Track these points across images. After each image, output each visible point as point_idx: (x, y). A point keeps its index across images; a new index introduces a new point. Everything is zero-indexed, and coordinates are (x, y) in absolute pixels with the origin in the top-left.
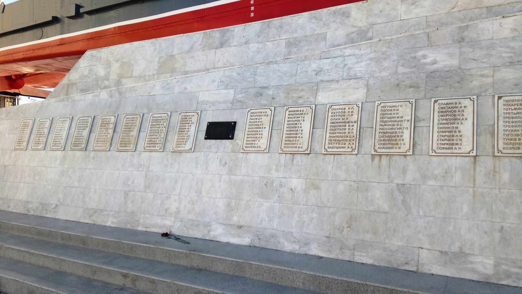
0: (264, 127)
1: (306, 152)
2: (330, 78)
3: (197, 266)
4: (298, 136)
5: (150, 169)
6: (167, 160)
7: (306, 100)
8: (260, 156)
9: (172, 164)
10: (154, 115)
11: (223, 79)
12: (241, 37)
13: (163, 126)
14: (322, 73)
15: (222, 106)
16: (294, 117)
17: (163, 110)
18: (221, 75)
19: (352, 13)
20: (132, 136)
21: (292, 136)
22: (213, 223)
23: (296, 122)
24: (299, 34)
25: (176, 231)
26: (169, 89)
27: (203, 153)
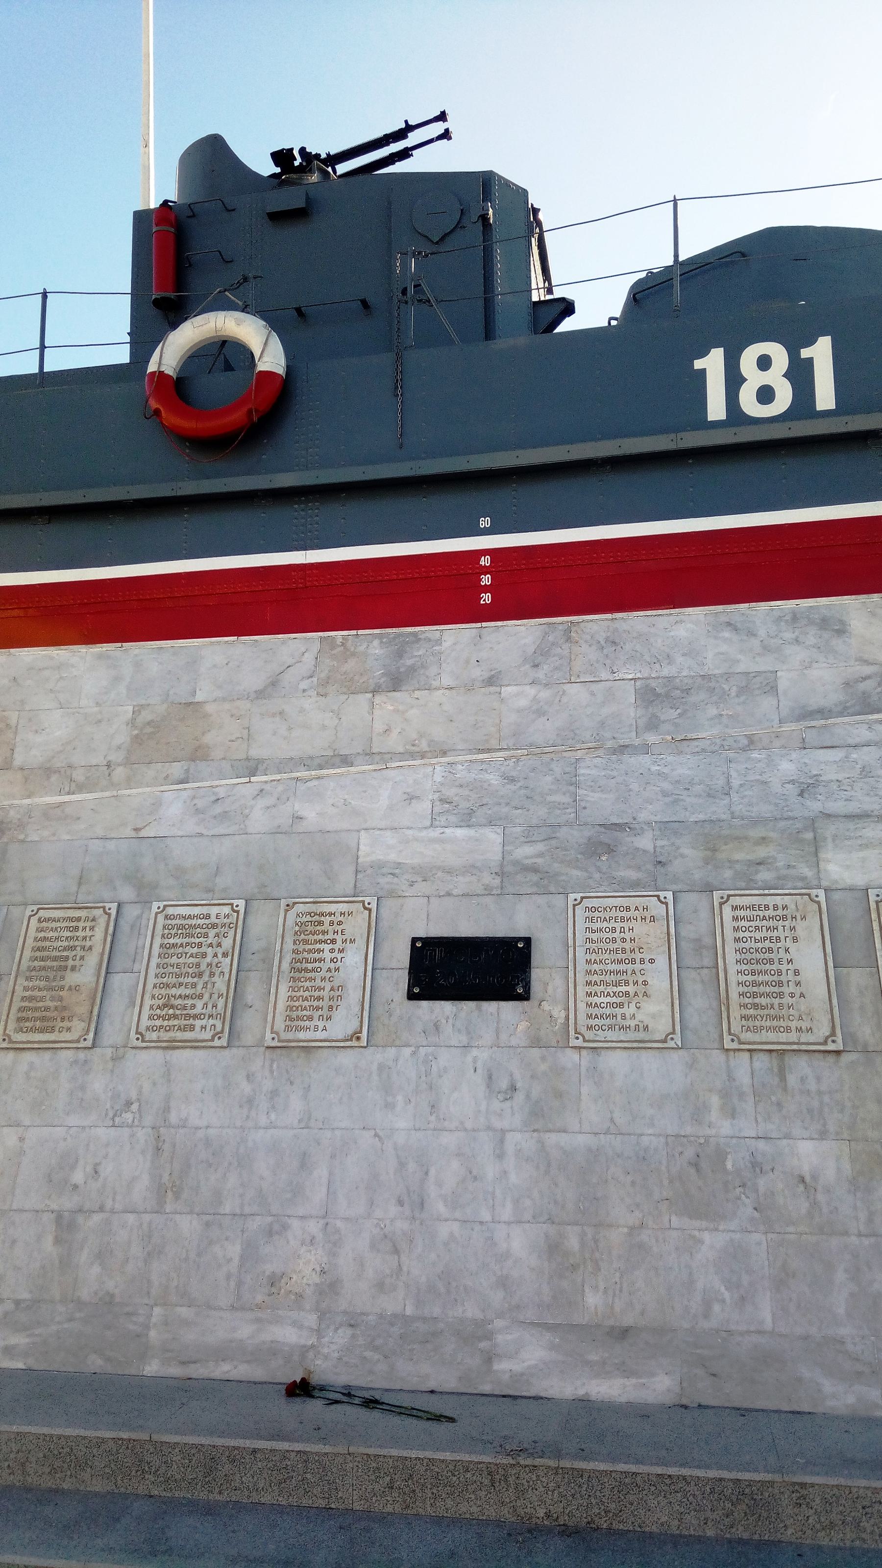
0: (647, 957)
1: (831, 1047)
2: (853, 808)
3: (548, 1515)
4: (786, 990)
5: (173, 1118)
6: (249, 1077)
7: (784, 872)
8: (650, 1061)
9: (274, 1093)
10: (170, 911)
11: (450, 792)
12: (467, 662)
13: (220, 951)
14: (821, 789)
15: (462, 883)
16: (757, 928)
17: (209, 890)
18: (438, 778)
19: (852, 623)
20: (76, 988)
21: (762, 989)
22: (499, 1323)
23: (767, 944)
24: (681, 668)
25: (327, 1369)
26: (224, 816)
27: (407, 1051)
